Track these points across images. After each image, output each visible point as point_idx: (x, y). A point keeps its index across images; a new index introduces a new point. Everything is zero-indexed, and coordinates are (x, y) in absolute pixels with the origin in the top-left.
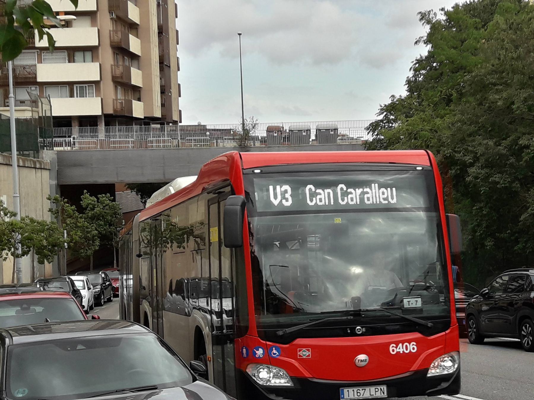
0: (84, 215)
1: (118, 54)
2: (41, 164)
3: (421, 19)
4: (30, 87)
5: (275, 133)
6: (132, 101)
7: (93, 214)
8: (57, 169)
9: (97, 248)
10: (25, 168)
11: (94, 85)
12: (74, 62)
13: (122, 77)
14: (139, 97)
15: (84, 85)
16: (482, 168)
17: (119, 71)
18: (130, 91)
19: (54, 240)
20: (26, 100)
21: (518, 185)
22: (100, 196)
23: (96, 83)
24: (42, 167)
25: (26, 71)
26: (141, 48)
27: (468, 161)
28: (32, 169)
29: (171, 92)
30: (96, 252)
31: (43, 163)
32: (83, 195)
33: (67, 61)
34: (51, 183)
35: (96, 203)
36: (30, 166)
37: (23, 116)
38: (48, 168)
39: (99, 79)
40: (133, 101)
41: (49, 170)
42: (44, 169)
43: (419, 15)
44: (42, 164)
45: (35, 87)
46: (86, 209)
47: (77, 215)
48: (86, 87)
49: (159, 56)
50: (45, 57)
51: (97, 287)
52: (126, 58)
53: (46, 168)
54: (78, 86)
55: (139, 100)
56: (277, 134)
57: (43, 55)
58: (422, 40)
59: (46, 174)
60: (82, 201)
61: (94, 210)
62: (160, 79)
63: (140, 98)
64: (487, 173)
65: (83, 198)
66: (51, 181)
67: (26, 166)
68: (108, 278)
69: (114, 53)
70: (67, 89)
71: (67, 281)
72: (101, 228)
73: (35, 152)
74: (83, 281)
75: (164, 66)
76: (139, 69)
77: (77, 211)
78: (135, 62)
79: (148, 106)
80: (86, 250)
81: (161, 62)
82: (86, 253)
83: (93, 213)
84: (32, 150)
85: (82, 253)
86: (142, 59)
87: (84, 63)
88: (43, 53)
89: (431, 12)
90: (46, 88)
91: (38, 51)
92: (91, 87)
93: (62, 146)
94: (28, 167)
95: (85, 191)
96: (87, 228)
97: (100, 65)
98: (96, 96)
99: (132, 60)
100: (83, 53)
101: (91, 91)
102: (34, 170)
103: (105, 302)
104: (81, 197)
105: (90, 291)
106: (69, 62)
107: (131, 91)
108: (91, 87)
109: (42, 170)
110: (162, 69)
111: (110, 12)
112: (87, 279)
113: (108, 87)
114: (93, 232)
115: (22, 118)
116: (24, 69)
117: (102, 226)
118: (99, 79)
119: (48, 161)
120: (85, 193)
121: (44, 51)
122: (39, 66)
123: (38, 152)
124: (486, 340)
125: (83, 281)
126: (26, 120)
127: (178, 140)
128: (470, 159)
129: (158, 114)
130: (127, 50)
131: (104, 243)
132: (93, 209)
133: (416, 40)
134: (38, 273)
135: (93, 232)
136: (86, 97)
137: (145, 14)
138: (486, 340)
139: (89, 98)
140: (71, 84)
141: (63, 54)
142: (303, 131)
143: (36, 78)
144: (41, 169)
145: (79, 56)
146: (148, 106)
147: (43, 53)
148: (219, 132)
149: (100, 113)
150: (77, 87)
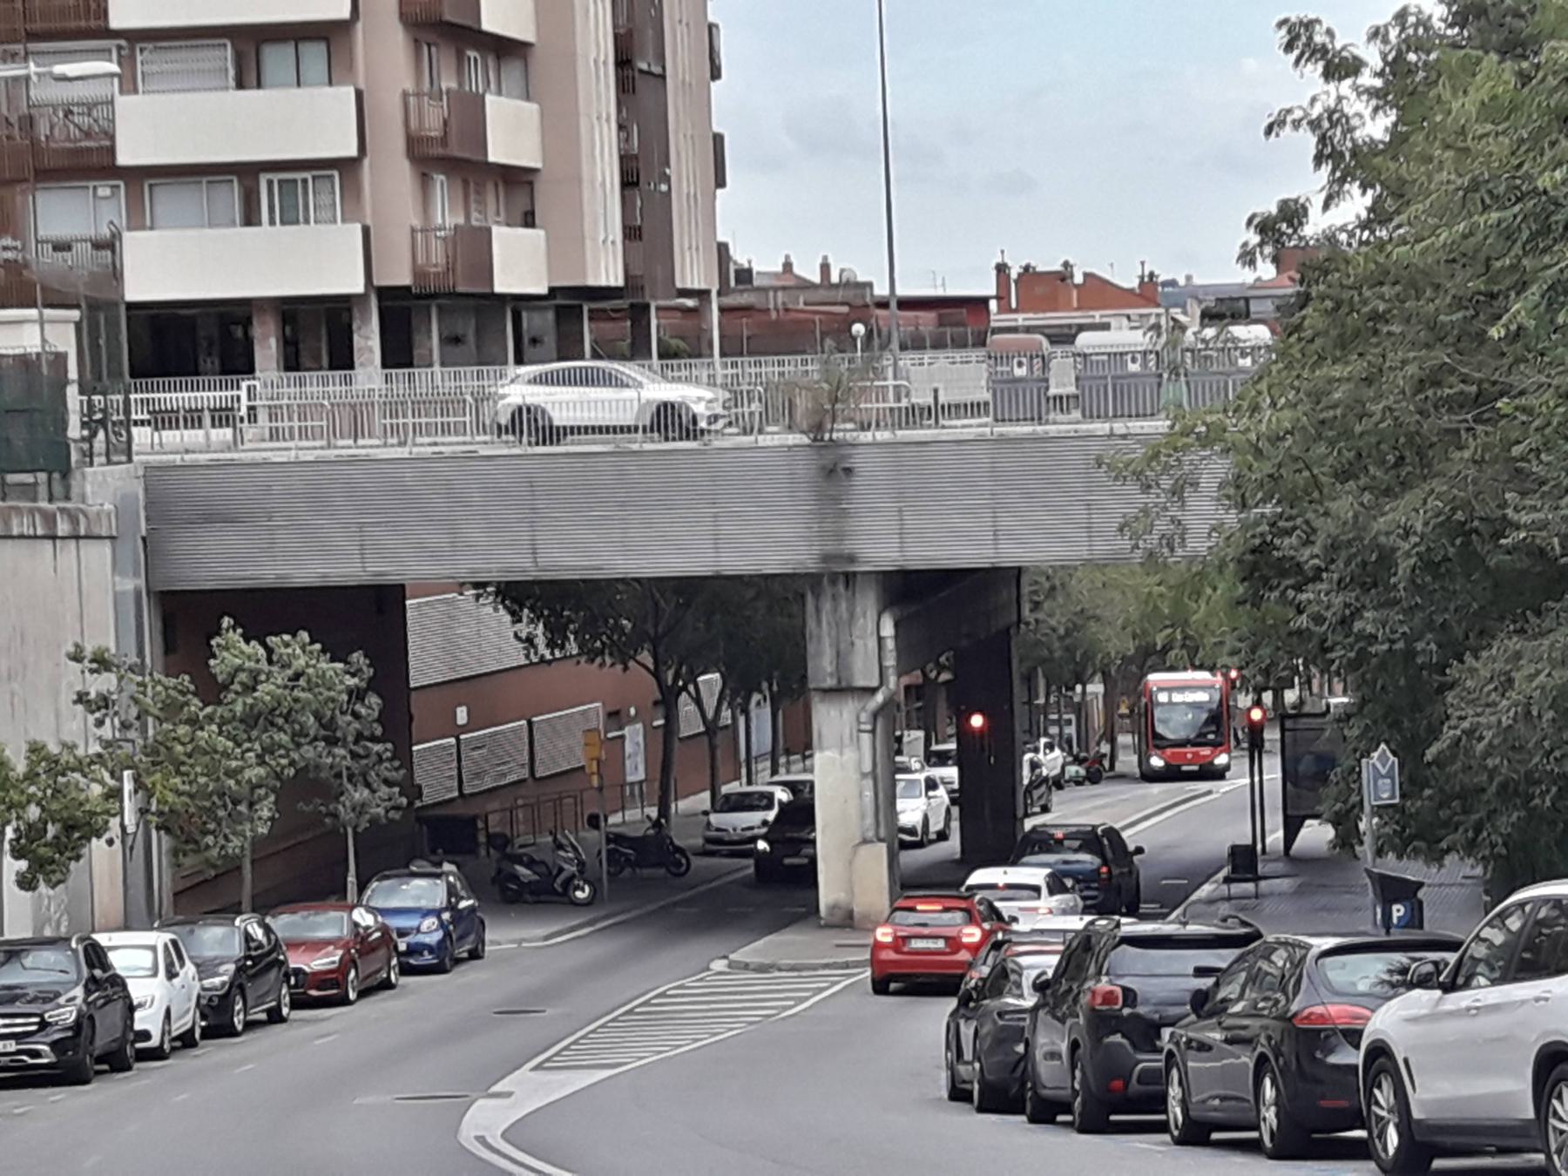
0: (220, 710)
1: (436, 45)
2: (73, 520)
3: (1289, 47)
4: (91, 184)
5: (1020, 364)
6: (489, 231)
7: (252, 706)
8: (144, 533)
9: (263, 830)
10: (10, 542)
11: (336, 174)
12: (259, 86)
13: (444, 142)
14: (529, 208)
15: (299, 176)
16: (1341, 585)
17: (432, 120)
18: (490, 187)
19: (66, 808)
20: (77, 241)
21: (1433, 646)
22: (274, 639)
23: (347, 167)
24: (82, 532)
25: (76, 125)
26: (537, 13)
27: (1307, 562)
28: (39, 542)
29: (667, 179)
30: (257, 842)
31: (86, 516)
32: (220, 635)
33: (232, 83)
34: (118, 588)
35: (264, 665)
36: (31, 532)
37: (14, 344)
38: (104, 533)
39: (352, 151)
40: (495, 230)
41: (112, 538)
42: (87, 537)
43: (1284, 31)
44: (82, 519)
45: (112, 187)
46: (225, 687)
47: (193, 708)
48: (305, 181)
49: (616, 37)
50: (146, 68)
51: (222, 969)
52: (472, 54)
53: (96, 531)
54: (276, 177)
55: (529, 220)
56: (1025, 368)
57: (139, 58)
58: (1289, 119)
59: (98, 555)
60: (214, 656)
61: (254, 690)
62: (621, 127)
63: (533, 213)
64: (1347, 605)
65: (219, 645)
66: (117, 579)
67: (15, 532)
68: (273, 937)
69: (417, 42)
70: (233, 194)
71: (75, 951)
72: (281, 756)
73: (56, 476)
74: (153, 949)
75: (637, 74)
76: (528, 98)
77: (195, 694)
78: (512, 71)
79: (566, 245)
80: (226, 838)
81: (623, 62)
82: (222, 847)
83: (249, 701)
84: (42, 470)
85: (208, 847)
86: (537, 58)
87: (295, 91)
88: (142, 50)
89: (1317, 27)
90: (157, 190)
91: (123, 43)
92: (324, 186)
93: (200, 426)
94: (22, 537)
95: (226, 621)
96: (226, 755)
97: (359, 95)
98: (344, 220)
99: (498, 58)
100: (293, 43)
101: (325, 199)
102: (48, 544)
103: (250, 1025)
104: (213, 642)
105: (175, 981)
106: (240, 85)
107: (496, 186)
108: (327, 180)
109: (82, 542)
110: (625, 86)
112: (174, 942)
114: (248, 774)
115: (11, 352)
116: (66, 116)
117: (285, 748)
118: (352, 151)
119: (108, 507)
120: (227, 630)
121: (143, 45)
122: (122, 102)
123: (66, 473)
124: (1215, 1136)
125: (153, 949)
127: (1463, 47)
128: (1317, 556)
129: (607, 271)
130: (470, 29)
131: (311, 807)
132: (250, 688)
133: (1271, 119)
134: (65, 917)
135: (248, 774)
136: (307, 221)
138: (1215, 1136)
139: (319, 226)
140: (247, 172)
141: (217, 53)
142: (1129, 357)
143: (112, 151)
144: (77, 538)
145: (277, 58)
147: (142, 50)
149: (358, 287)
150: (270, 183)
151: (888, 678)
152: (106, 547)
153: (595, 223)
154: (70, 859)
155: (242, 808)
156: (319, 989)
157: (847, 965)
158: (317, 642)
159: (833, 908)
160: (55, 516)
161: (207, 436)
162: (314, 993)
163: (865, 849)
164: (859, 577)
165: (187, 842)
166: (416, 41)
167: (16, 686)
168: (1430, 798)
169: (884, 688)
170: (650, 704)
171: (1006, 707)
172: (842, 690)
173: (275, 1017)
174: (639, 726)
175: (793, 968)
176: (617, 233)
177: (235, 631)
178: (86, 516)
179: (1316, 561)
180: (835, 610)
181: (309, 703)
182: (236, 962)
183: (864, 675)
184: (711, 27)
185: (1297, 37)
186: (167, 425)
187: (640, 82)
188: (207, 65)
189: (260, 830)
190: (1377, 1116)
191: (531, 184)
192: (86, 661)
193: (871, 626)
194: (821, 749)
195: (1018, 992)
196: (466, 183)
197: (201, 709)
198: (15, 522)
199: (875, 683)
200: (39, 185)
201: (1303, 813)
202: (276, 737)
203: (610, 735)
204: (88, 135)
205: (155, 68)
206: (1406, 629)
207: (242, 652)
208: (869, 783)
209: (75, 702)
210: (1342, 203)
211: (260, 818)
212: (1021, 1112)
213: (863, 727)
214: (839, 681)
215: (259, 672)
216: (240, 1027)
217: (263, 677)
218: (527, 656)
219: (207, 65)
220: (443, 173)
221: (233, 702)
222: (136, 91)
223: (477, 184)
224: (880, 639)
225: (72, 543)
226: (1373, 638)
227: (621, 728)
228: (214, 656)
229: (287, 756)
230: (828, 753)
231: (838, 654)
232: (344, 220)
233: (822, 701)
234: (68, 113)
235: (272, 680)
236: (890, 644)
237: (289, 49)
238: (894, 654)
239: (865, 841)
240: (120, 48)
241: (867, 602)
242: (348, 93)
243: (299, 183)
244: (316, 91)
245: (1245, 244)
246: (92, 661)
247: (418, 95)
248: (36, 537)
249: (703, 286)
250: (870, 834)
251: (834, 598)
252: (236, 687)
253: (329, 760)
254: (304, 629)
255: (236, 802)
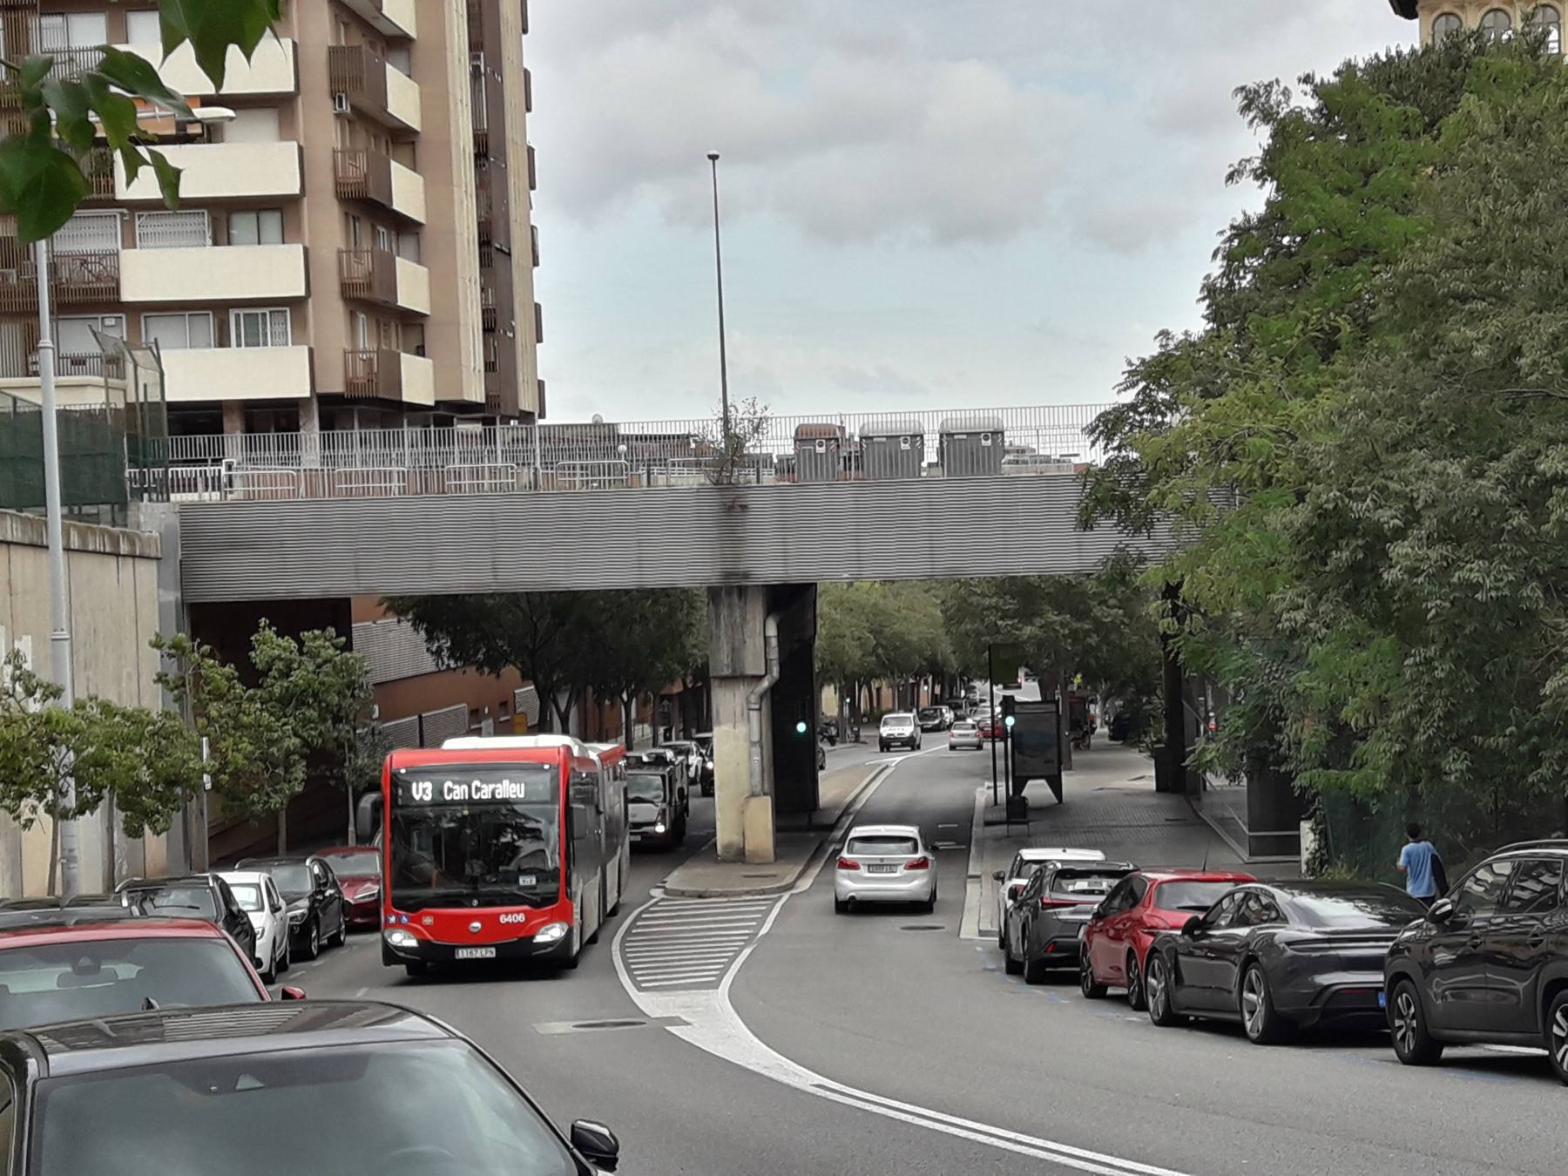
0: (259, 692)
1: (359, 219)
2: (132, 543)
3: (1246, 108)
4: (100, 316)
6: (399, 355)
9: (299, 789)
10: (85, 556)
12: (229, 243)
13: (369, 286)
14: (420, 344)
15: (259, 311)
16: (1431, 541)
17: (360, 271)
21: (1539, 593)
22: (306, 633)
23: (296, 304)
24: (138, 553)
25: (90, 272)
29: (513, 329)
30: (295, 799)
31: (140, 540)
32: (258, 632)
33: (209, 241)
34: (162, 599)
35: (296, 655)
38: (153, 555)
40: (403, 355)
41: (158, 559)
42: (141, 557)
43: (1240, 97)
46: (265, 674)
47: (238, 691)
52: (382, 230)
53: (147, 552)
54: (242, 312)
55: (420, 351)
56: (824, 447)
57: (137, 223)
60: (253, 649)
61: (288, 676)
62: (482, 290)
63: (423, 347)
66: (161, 592)
67: (91, 548)
70: (209, 324)
71: (211, 888)
74: (258, 886)
76: (419, 262)
78: (408, 243)
79: (447, 370)
80: (268, 794)
81: (485, 242)
82: (266, 803)
85: (253, 803)
86: (426, 234)
88: (139, 217)
91: (125, 211)
93: (196, 491)
94: (94, 552)
96: (269, 729)
98: (293, 344)
102: (113, 560)
104: (252, 638)
107: (397, 327)
110: (485, 262)
111: (335, 97)
113: (330, 314)
115: (77, 408)
118: (302, 293)
120: (264, 629)
121: (140, 213)
124: (1447, 1052)
125: (258, 886)
126: (89, 414)
127: (536, 469)
130: (383, 205)
132: (286, 674)
133: (1232, 169)
134: (125, 863)
137: (436, 101)
138: (1447, 1052)
140: (220, 308)
141: (198, 219)
143: (117, 290)
144: (134, 557)
145: (243, 224)
146: (447, 370)
148: (655, 445)
149: (305, 392)
150: (238, 316)
151: (771, 667)
152: (153, 565)
153: (468, 358)
154: (172, 810)
155: (280, 771)
156: (362, 917)
157: (763, 892)
158: (341, 636)
159: (727, 847)
160: (119, 538)
161: (200, 496)
162: (359, 920)
163: (754, 801)
164: (750, 592)
165: (233, 800)
166: (346, 214)
167: (90, 673)
168: (1512, 734)
169: (768, 676)
170: (497, 704)
171: (808, 697)
172: (736, 678)
173: (335, 943)
174: (491, 721)
175: (721, 895)
176: (481, 365)
177: (270, 629)
178: (140, 540)
179: (1396, 521)
180: (731, 615)
181: (332, 685)
182: (309, 897)
183: (753, 665)
184: (533, 228)
185: (1251, 102)
186: (176, 489)
187: (495, 256)
188: (189, 229)
189: (297, 789)
190: (1249, 1002)
191: (422, 325)
192: (165, 647)
193: (759, 627)
194: (719, 724)
195: (1274, 915)
196: (378, 322)
197: (245, 692)
198: (90, 539)
199: (763, 673)
200: (60, 317)
201: (1025, 774)
202: (308, 714)
203: (473, 727)
204: (98, 278)
205: (150, 230)
206: (1511, 577)
207: (279, 646)
208: (757, 750)
209: (155, 682)
210: (153, 661)
211: (296, 779)
212: (1385, 1041)
213: (753, 706)
214: (734, 670)
215: (292, 661)
216: (315, 952)
217: (295, 666)
218: (437, 665)
219: (189, 229)
220: (363, 312)
221: (272, 685)
222: (135, 247)
223: (385, 325)
224: (766, 638)
225: (130, 560)
226: (1477, 587)
227: (480, 722)
228: (253, 649)
229: (316, 729)
230: (724, 728)
231: (733, 649)
232: (293, 344)
233: (720, 686)
234: (84, 262)
235: (303, 667)
236: (774, 642)
237: (253, 216)
238: (777, 649)
239: (753, 795)
240: (122, 215)
241: (756, 609)
242: (298, 249)
243: (260, 317)
244: (272, 247)
245: (1208, 277)
246: (170, 648)
247: (348, 252)
248: (104, 553)
249: (531, 410)
250: (758, 789)
251: (730, 606)
252: (273, 673)
253: (336, 734)
254: (332, 625)
255: (276, 766)
